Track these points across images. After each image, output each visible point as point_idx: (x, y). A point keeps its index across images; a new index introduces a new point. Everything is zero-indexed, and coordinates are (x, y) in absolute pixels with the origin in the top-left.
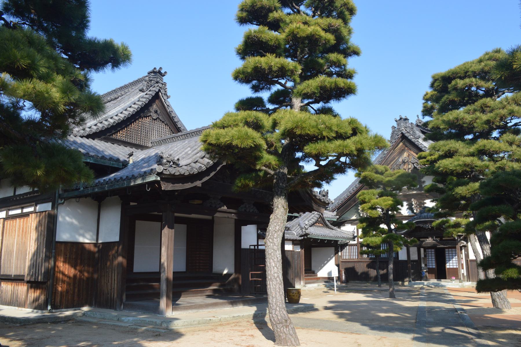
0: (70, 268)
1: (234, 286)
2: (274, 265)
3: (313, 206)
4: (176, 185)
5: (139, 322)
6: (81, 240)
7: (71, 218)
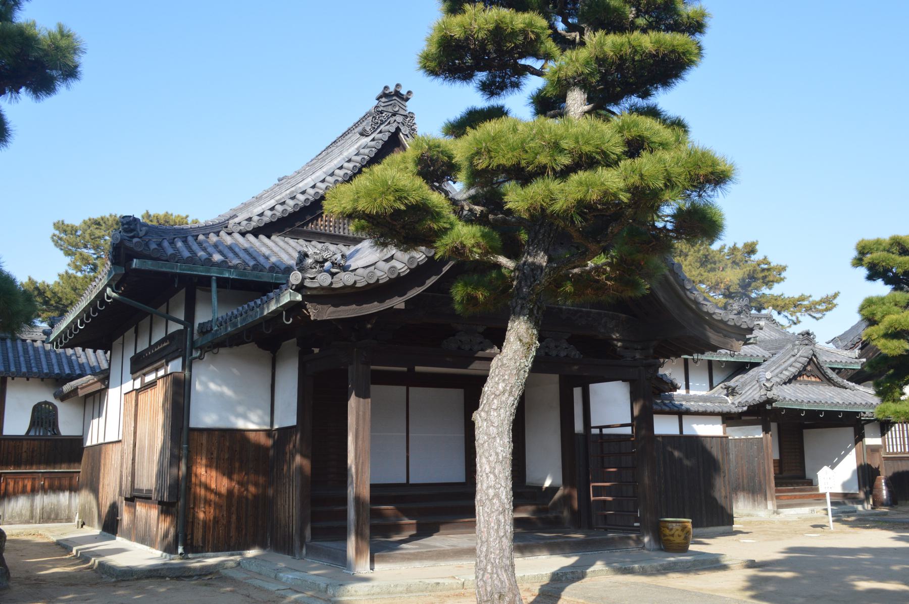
0: (220, 477)
1: (562, 513)
2: (488, 470)
3: (708, 338)
4: (342, 308)
5: (299, 582)
6: (241, 424)
7: (220, 386)
